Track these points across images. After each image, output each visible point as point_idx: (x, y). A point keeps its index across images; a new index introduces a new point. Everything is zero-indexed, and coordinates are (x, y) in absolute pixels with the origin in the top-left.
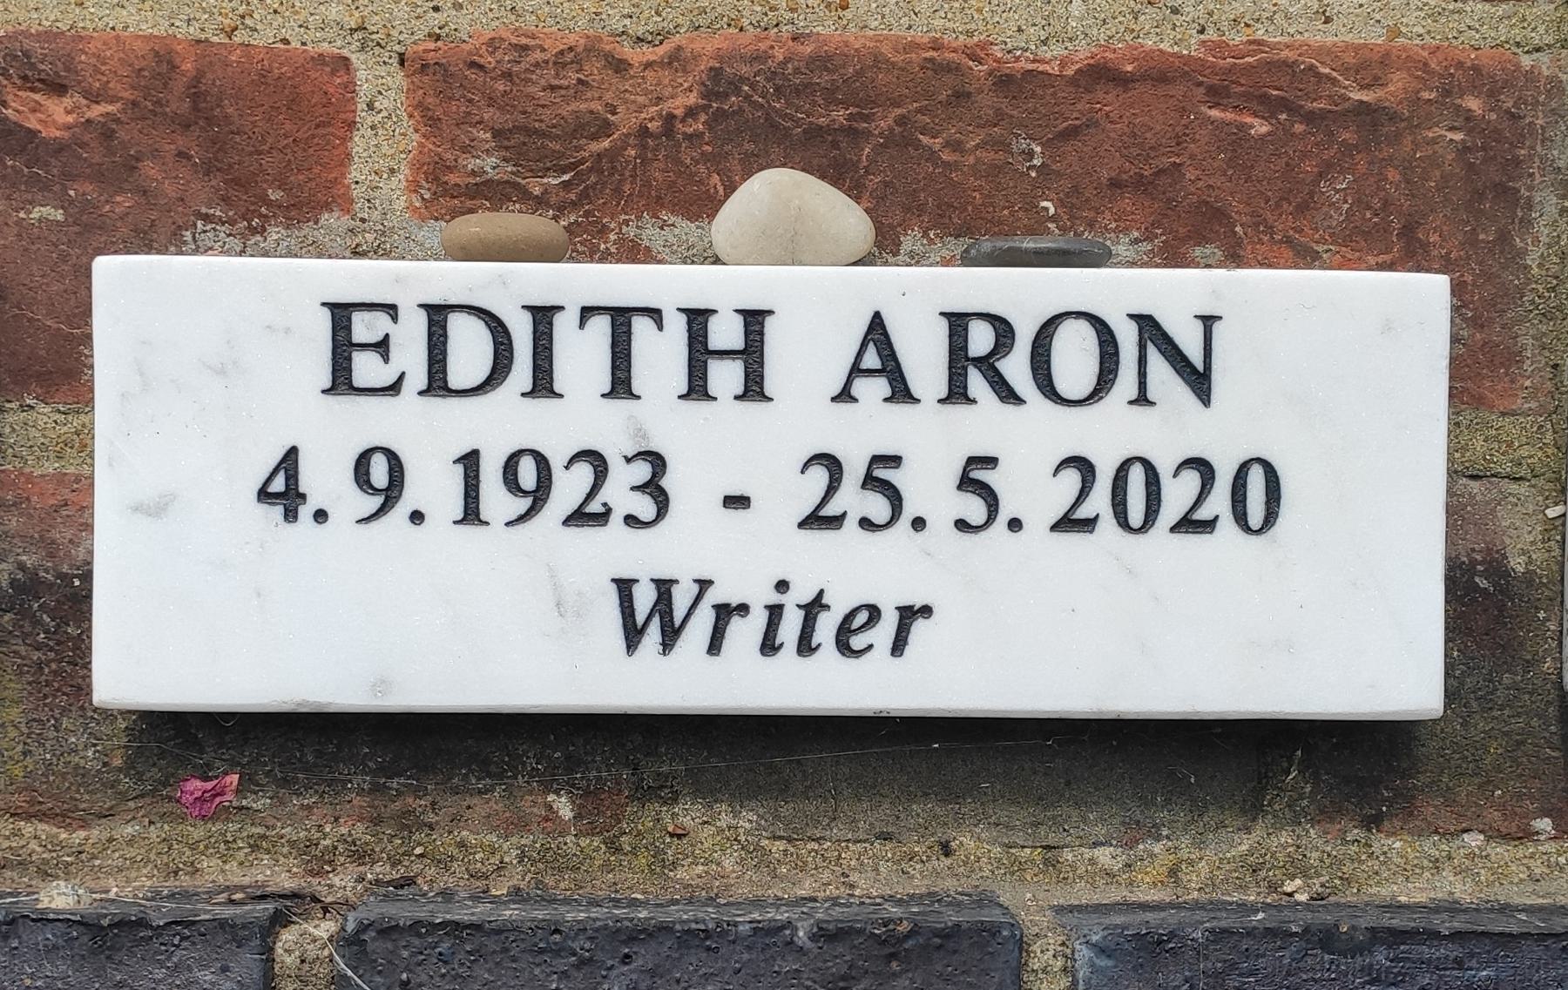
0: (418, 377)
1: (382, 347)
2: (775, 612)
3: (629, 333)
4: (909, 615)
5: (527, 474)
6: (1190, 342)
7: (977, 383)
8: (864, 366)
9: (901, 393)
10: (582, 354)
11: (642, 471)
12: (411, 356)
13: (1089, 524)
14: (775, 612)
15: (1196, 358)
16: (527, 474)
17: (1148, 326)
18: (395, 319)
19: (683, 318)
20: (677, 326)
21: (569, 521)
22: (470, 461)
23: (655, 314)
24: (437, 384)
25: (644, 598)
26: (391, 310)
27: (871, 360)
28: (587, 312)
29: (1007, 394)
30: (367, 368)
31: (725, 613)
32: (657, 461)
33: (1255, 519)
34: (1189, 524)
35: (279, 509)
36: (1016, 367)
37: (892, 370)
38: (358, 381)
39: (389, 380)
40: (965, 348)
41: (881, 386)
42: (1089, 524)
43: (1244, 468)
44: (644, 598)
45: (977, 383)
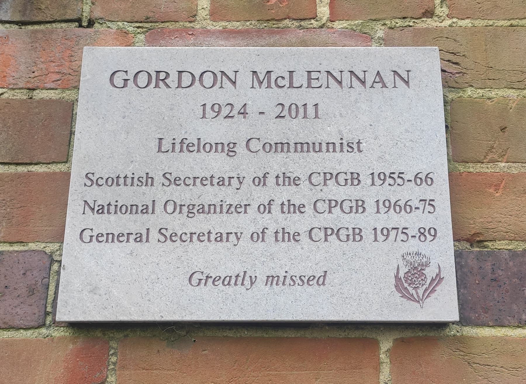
6: (405, 75)
8: (376, 81)
15: (406, 79)
16: (216, 108)
24: (291, 86)
27: (378, 80)
30: (314, 83)
37: (382, 81)
41: (380, 85)
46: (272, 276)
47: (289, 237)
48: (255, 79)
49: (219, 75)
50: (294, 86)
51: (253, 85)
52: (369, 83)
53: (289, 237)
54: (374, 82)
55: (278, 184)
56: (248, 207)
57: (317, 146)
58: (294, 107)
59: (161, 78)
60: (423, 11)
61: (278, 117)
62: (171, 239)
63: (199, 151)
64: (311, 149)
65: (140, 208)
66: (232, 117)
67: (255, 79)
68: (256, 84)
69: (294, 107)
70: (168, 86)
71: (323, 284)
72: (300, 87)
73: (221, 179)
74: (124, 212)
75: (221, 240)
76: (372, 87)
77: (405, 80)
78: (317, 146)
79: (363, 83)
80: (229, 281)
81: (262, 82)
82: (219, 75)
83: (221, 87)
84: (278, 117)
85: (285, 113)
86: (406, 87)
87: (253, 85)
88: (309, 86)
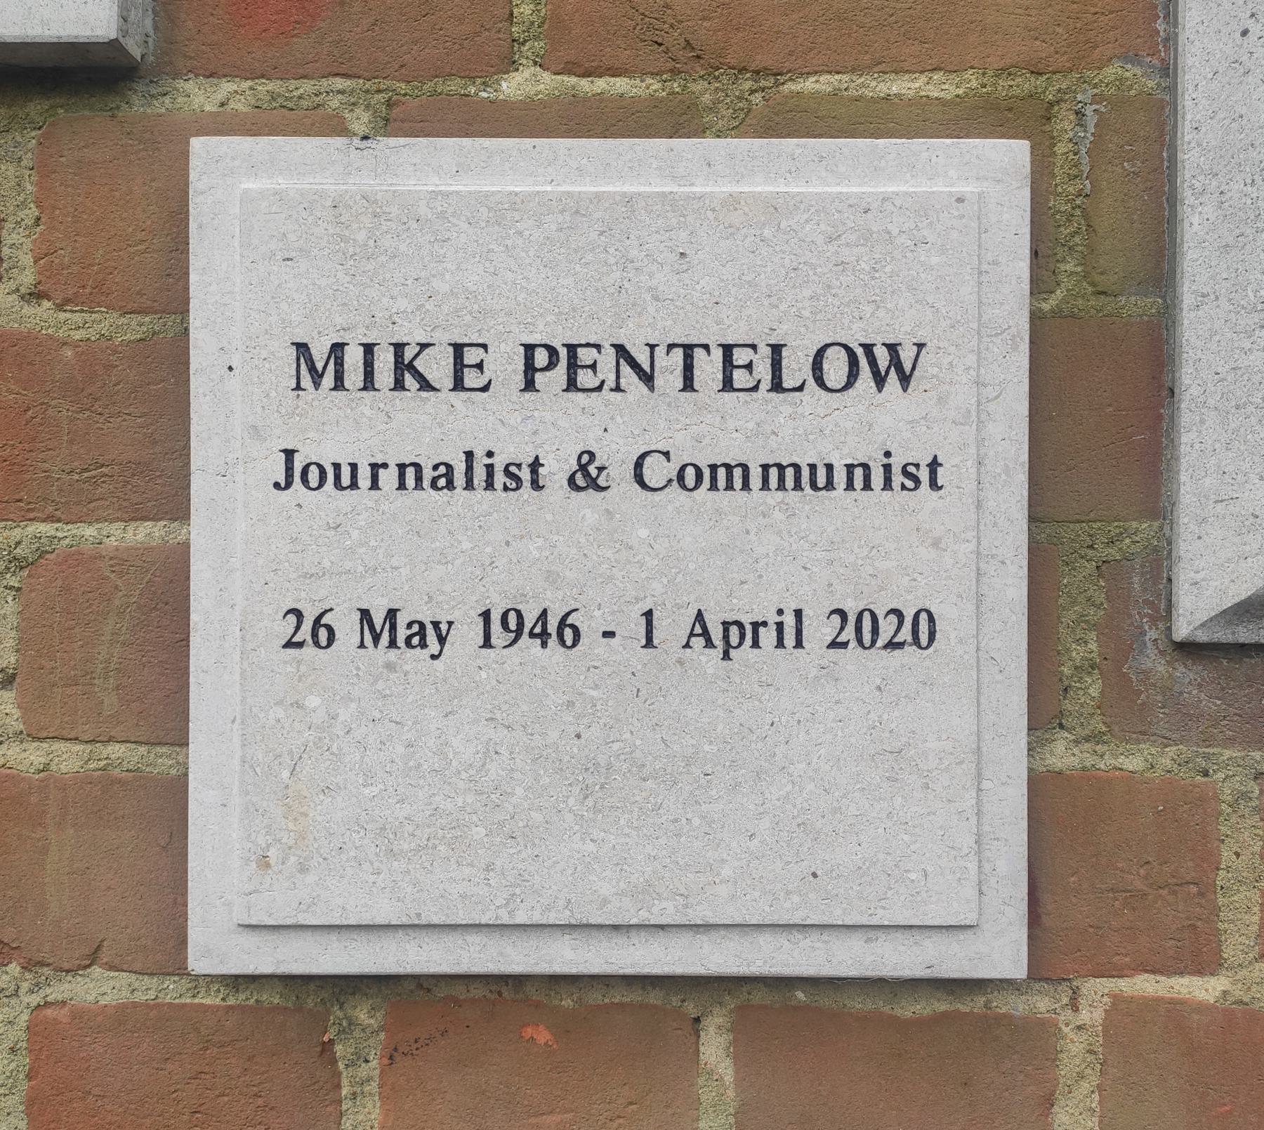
0: (766, 384)
1: (749, 367)
2: (780, 626)
3: (692, 357)
6: (643, 358)
12: (763, 371)
13: (844, 645)
15: (646, 367)
18: (599, 352)
19: (721, 349)
20: (718, 354)
21: (885, 647)
23: (706, 347)
24: (777, 386)
26: (598, 347)
28: (671, 347)
30: (740, 378)
33: (924, 616)
34: (892, 645)
35: (539, 641)
38: (736, 386)
39: (597, 384)
40: (462, 360)
42: (844, 645)
43: (320, 486)
47: (338, 477)
48: (303, 367)
50: (736, 386)
51: (298, 383)
53: (338, 477)
56: (381, 471)
59: (740, 363)
60: (319, 1049)
64: (805, 473)
65: (428, 474)
67: (303, 367)
68: (306, 381)
70: (425, 385)
73: (442, 470)
74: (314, 470)
75: (450, 485)
77: (642, 370)
81: (321, 376)
86: (645, 390)
87: (298, 383)
88: (458, 385)
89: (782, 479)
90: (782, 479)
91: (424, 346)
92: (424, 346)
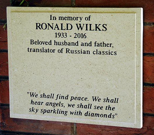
2: (75, 112)
4: (42, 103)
5: (59, 34)
7: (38, 28)
9: (58, 29)
10: (65, 27)
11: (65, 34)
13: (76, 37)
14: (75, 112)
16: (59, 34)
17: (49, 24)
22: (56, 33)
25: (94, 98)
27: (56, 27)
29: (40, 29)
31: (51, 111)
32: (66, 34)
36: (40, 27)
37: (58, 27)
38: (92, 30)
41: (57, 29)
44: (94, 98)
45: (38, 28)
46: (97, 114)
49: (47, 25)
52: (54, 28)
54: (55, 28)
55: (28, 51)
57: (86, 45)
58: (79, 34)
61: (75, 37)
62: (97, 108)
63: (38, 44)
66: (76, 37)
69: (79, 34)
71: (72, 97)
72: (94, 30)
76: (55, 29)
78: (86, 45)
79: (52, 28)
80: (48, 104)
82: (47, 25)
83: (48, 29)
84: (75, 37)
85: (77, 36)
89: (61, 18)
90: (61, 18)
91: (99, 25)
92: (99, 25)
